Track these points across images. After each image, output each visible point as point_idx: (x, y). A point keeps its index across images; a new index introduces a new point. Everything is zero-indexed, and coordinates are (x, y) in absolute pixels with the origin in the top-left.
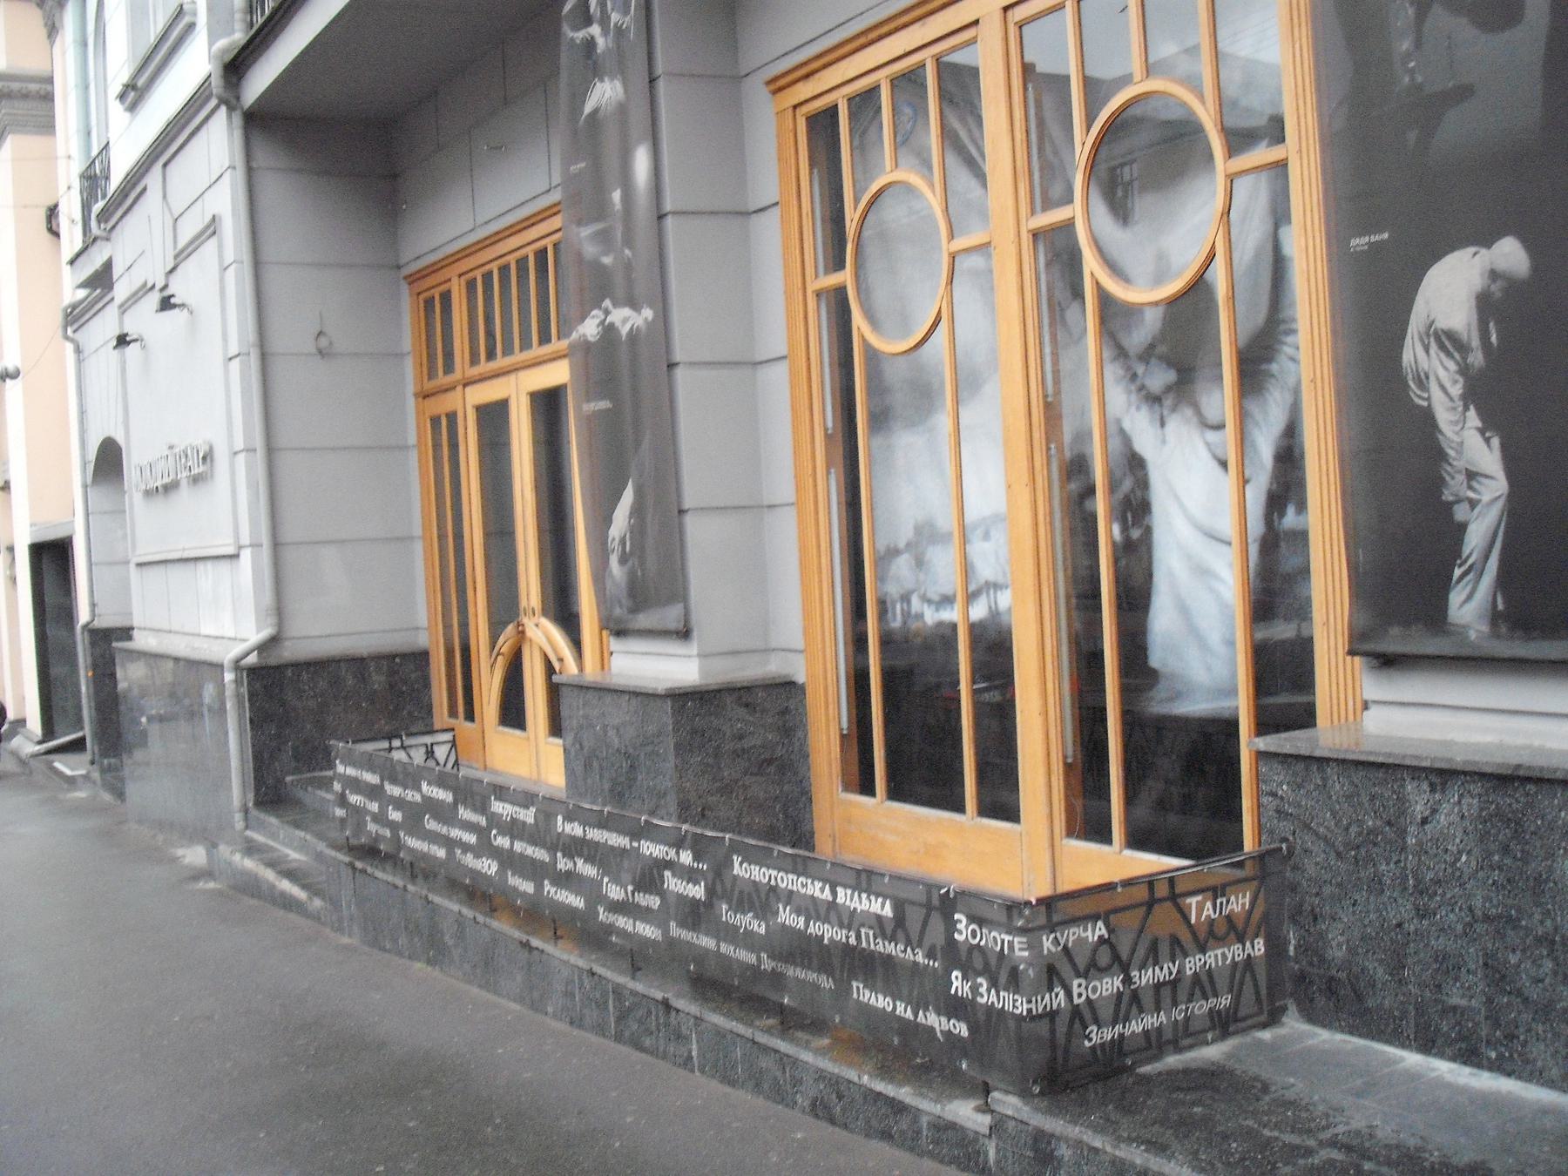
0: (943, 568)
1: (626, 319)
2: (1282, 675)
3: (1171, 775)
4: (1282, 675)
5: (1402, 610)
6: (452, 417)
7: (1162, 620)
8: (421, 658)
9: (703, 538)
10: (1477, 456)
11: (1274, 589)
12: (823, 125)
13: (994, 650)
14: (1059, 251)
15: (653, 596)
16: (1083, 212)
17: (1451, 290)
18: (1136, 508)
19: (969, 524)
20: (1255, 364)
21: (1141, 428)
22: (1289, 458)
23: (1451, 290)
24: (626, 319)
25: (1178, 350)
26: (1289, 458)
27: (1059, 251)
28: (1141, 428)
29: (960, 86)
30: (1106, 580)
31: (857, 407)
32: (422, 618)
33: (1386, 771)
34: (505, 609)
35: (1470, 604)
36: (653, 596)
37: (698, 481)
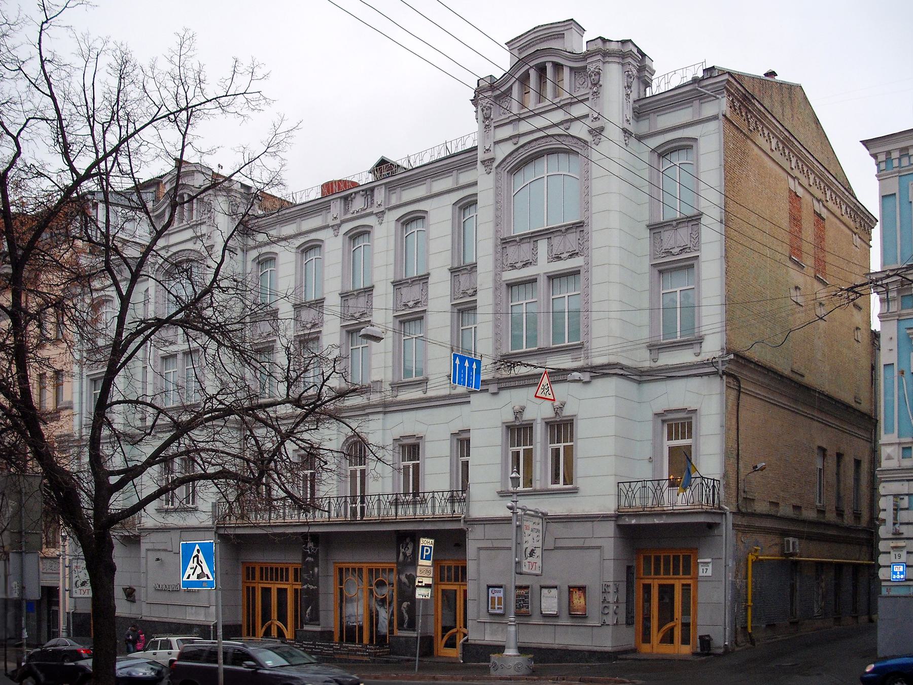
0: (353, 619)
1: (311, 587)
2: (391, 632)
3: (381, 640)
4: (391, 632)
5: (400, 626)
6: (254, 588)
7: (379, 626)
8: (241, 626)
9: (322, 614)
10: (406, 616)
11: (391, 623)
12: (341, 570)
13: (361, 628)
14: (371, 591)
15: (315, 619)
16: (374, 587)
17: (405, 604)
18: (377, 615)
19: (357, 612)
20: (390, 603)
21: (378, 608)
22: (393, 612)
23: (405, 604)
24: (311, 587)
25: (382, 602)
26: (393, 612)
27: (371, 591)
28: (378, 608)
29: (360, 570)
30: (373, 618)
31: (342, 599)
32: (240, 618)
33: (400, 637)
34: (266, 616)
35: (405, 626)
36: (315, 619)
37: (322, 606)
